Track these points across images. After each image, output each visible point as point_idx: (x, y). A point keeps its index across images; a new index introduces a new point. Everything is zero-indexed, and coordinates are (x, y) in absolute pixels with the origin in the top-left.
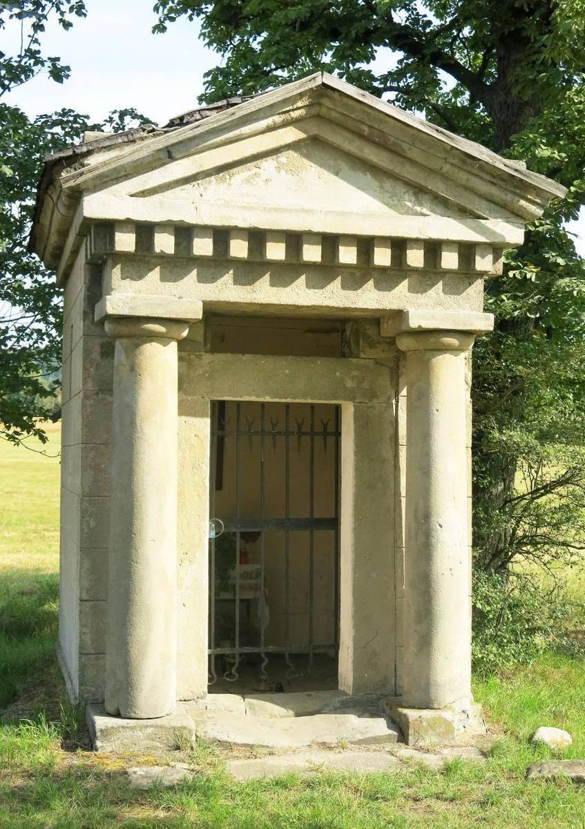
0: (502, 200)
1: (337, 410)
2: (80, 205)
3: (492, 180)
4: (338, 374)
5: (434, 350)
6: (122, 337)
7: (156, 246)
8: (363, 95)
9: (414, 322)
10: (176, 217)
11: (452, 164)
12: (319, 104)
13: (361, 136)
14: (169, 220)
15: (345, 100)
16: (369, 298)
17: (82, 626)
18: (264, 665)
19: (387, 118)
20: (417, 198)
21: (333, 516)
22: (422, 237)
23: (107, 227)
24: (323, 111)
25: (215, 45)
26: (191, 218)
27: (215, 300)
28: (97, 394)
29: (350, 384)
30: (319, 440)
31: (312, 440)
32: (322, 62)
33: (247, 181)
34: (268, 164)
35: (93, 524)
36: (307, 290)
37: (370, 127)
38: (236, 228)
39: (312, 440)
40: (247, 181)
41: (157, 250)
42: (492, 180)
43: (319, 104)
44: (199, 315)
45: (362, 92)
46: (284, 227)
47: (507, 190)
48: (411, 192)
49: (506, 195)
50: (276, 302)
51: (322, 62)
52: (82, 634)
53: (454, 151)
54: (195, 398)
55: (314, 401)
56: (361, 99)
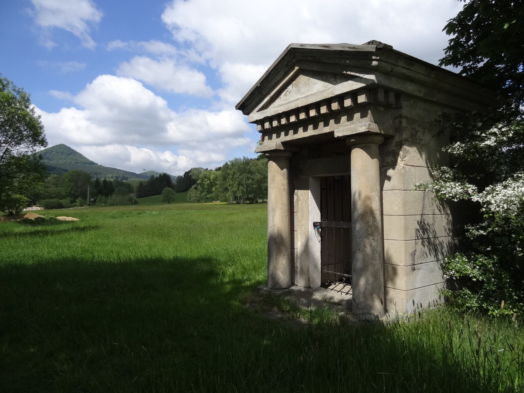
9: (336, 135)
16: (322, 129)
22: (333, 96)
34: (290, 87)
40: (285, 95)
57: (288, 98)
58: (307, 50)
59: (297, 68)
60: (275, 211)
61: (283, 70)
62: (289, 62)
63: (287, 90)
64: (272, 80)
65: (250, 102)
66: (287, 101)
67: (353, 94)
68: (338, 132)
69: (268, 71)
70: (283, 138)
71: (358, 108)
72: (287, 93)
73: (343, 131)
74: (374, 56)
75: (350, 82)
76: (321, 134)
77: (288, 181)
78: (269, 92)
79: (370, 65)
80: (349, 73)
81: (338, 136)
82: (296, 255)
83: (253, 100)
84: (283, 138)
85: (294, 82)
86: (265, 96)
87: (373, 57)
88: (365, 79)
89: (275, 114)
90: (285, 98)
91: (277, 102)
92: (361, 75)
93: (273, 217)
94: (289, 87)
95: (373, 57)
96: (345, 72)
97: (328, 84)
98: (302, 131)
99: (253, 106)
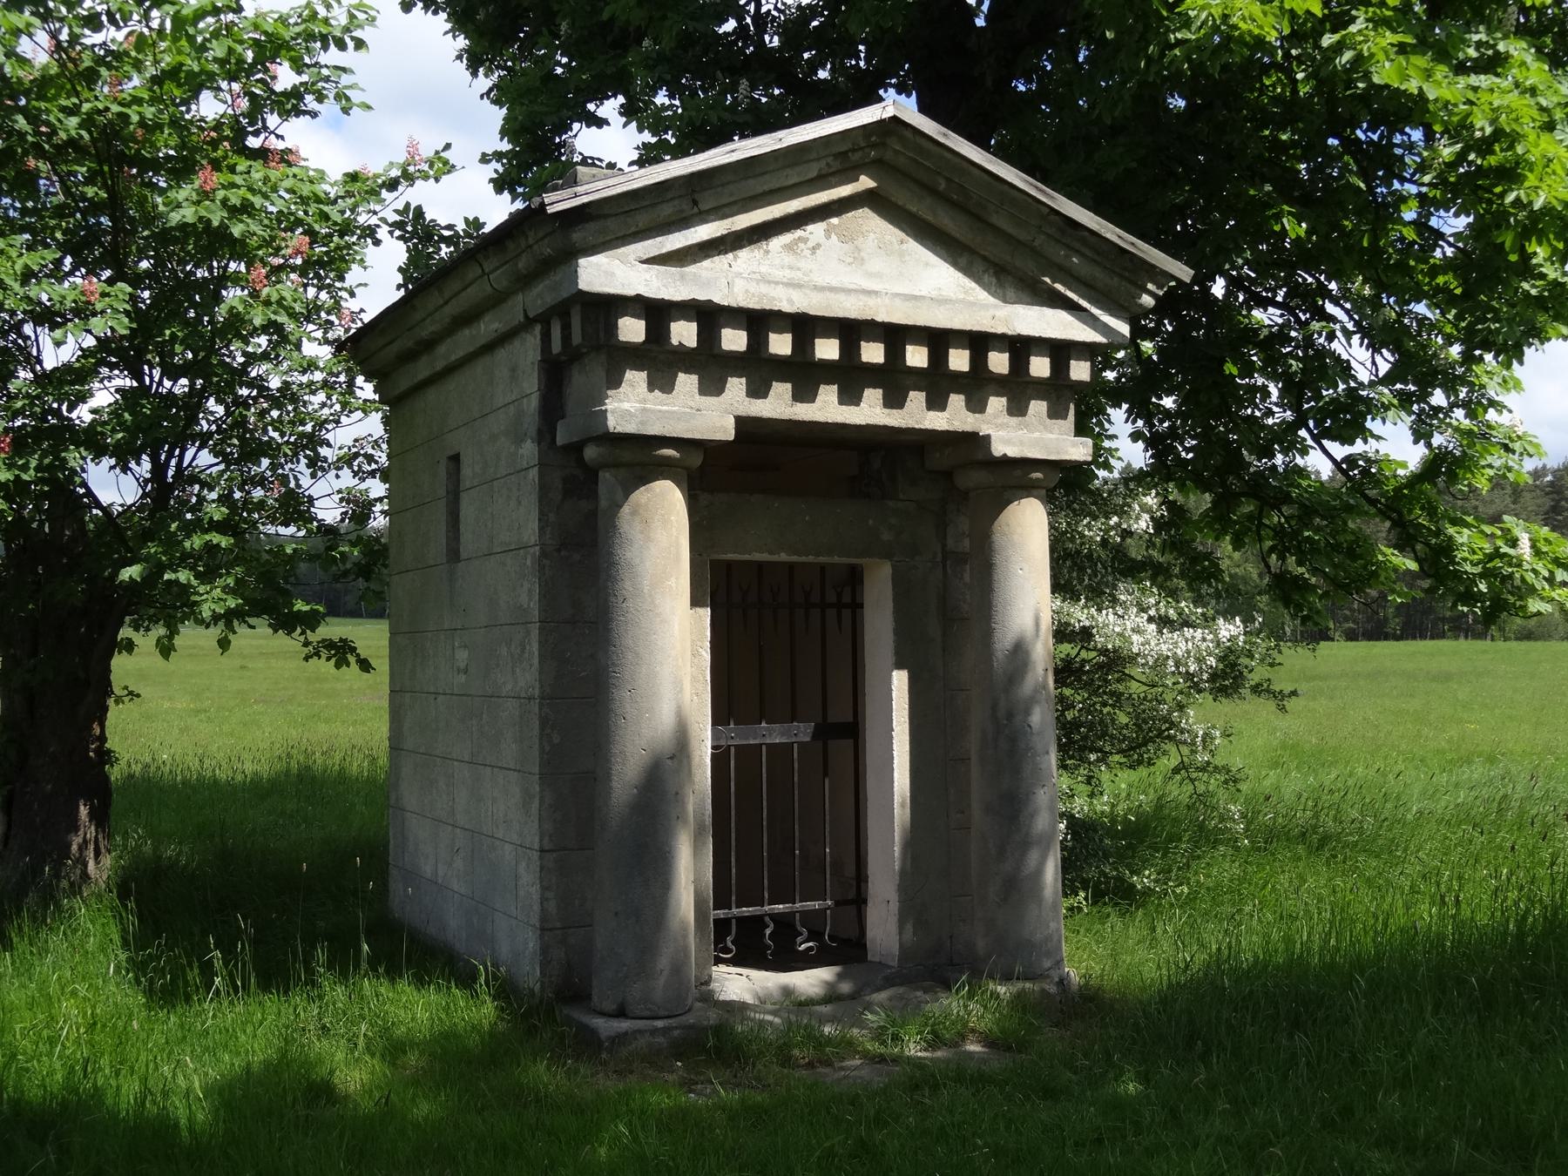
3: (1096, 257)
4: (871, 522)
5: (1011, 487)
7: (672, 336)
8: (945, 135)
11: (1049, 236)
12: (884, 144)
13: (933, 191)
14: (694, 300)
16: (954, 416)
17: (544, 889)
18: (768, 932)
19: (972, 169)
20: (998, 279)
21: (851, 719)
22: (1010, 333)
23: (612, 306)
24: (889, 156)
26: (721, 298)
28: (559, 550)
29: (886, 536)
30: (831, 614)
32: (505, 146)
33: (789, 248)
34: (816, 230)
35: (556, 739)
37: (949, 180)
38: (779, 314)
40: (789, 248)
41: (675, 342)
42: (1096, 257)
43: (884, 144)
45: (944, 130)
46: (841, 314)
48: (991, 271)
50: (822, 419)
51: (505, 146)
52: (543, 900)
53: (1052, 217)
55: (795, 558)
56: (942, 140)
57: (802, 264)
59: (865, 182)
61: (823, 164)
62: (853, 150)
63: (799, 233)
66: (797, 276)
67: (1061, 351)
68: (1008, 442)
71: (1058, 391)
72: (801, 245)
73: (1022, 443)
75: (1062, 316)
77: (611, 554)
78: (726, 210)
79: (1134, 298)
80: (1058, 286)
82: (704, 843)
84: (736, 398)
85: (835, 221)
86: (703, 217)
87: (1150, 286)
88: (1105, 325)
89: (757, 307)
90: (788, 259)
91: (746, 258)
94: (810, 228)
95: (1150, 286)
96: (1047, 280)
97: (973, 285)
98: (835, 398)
99: (633, 229)
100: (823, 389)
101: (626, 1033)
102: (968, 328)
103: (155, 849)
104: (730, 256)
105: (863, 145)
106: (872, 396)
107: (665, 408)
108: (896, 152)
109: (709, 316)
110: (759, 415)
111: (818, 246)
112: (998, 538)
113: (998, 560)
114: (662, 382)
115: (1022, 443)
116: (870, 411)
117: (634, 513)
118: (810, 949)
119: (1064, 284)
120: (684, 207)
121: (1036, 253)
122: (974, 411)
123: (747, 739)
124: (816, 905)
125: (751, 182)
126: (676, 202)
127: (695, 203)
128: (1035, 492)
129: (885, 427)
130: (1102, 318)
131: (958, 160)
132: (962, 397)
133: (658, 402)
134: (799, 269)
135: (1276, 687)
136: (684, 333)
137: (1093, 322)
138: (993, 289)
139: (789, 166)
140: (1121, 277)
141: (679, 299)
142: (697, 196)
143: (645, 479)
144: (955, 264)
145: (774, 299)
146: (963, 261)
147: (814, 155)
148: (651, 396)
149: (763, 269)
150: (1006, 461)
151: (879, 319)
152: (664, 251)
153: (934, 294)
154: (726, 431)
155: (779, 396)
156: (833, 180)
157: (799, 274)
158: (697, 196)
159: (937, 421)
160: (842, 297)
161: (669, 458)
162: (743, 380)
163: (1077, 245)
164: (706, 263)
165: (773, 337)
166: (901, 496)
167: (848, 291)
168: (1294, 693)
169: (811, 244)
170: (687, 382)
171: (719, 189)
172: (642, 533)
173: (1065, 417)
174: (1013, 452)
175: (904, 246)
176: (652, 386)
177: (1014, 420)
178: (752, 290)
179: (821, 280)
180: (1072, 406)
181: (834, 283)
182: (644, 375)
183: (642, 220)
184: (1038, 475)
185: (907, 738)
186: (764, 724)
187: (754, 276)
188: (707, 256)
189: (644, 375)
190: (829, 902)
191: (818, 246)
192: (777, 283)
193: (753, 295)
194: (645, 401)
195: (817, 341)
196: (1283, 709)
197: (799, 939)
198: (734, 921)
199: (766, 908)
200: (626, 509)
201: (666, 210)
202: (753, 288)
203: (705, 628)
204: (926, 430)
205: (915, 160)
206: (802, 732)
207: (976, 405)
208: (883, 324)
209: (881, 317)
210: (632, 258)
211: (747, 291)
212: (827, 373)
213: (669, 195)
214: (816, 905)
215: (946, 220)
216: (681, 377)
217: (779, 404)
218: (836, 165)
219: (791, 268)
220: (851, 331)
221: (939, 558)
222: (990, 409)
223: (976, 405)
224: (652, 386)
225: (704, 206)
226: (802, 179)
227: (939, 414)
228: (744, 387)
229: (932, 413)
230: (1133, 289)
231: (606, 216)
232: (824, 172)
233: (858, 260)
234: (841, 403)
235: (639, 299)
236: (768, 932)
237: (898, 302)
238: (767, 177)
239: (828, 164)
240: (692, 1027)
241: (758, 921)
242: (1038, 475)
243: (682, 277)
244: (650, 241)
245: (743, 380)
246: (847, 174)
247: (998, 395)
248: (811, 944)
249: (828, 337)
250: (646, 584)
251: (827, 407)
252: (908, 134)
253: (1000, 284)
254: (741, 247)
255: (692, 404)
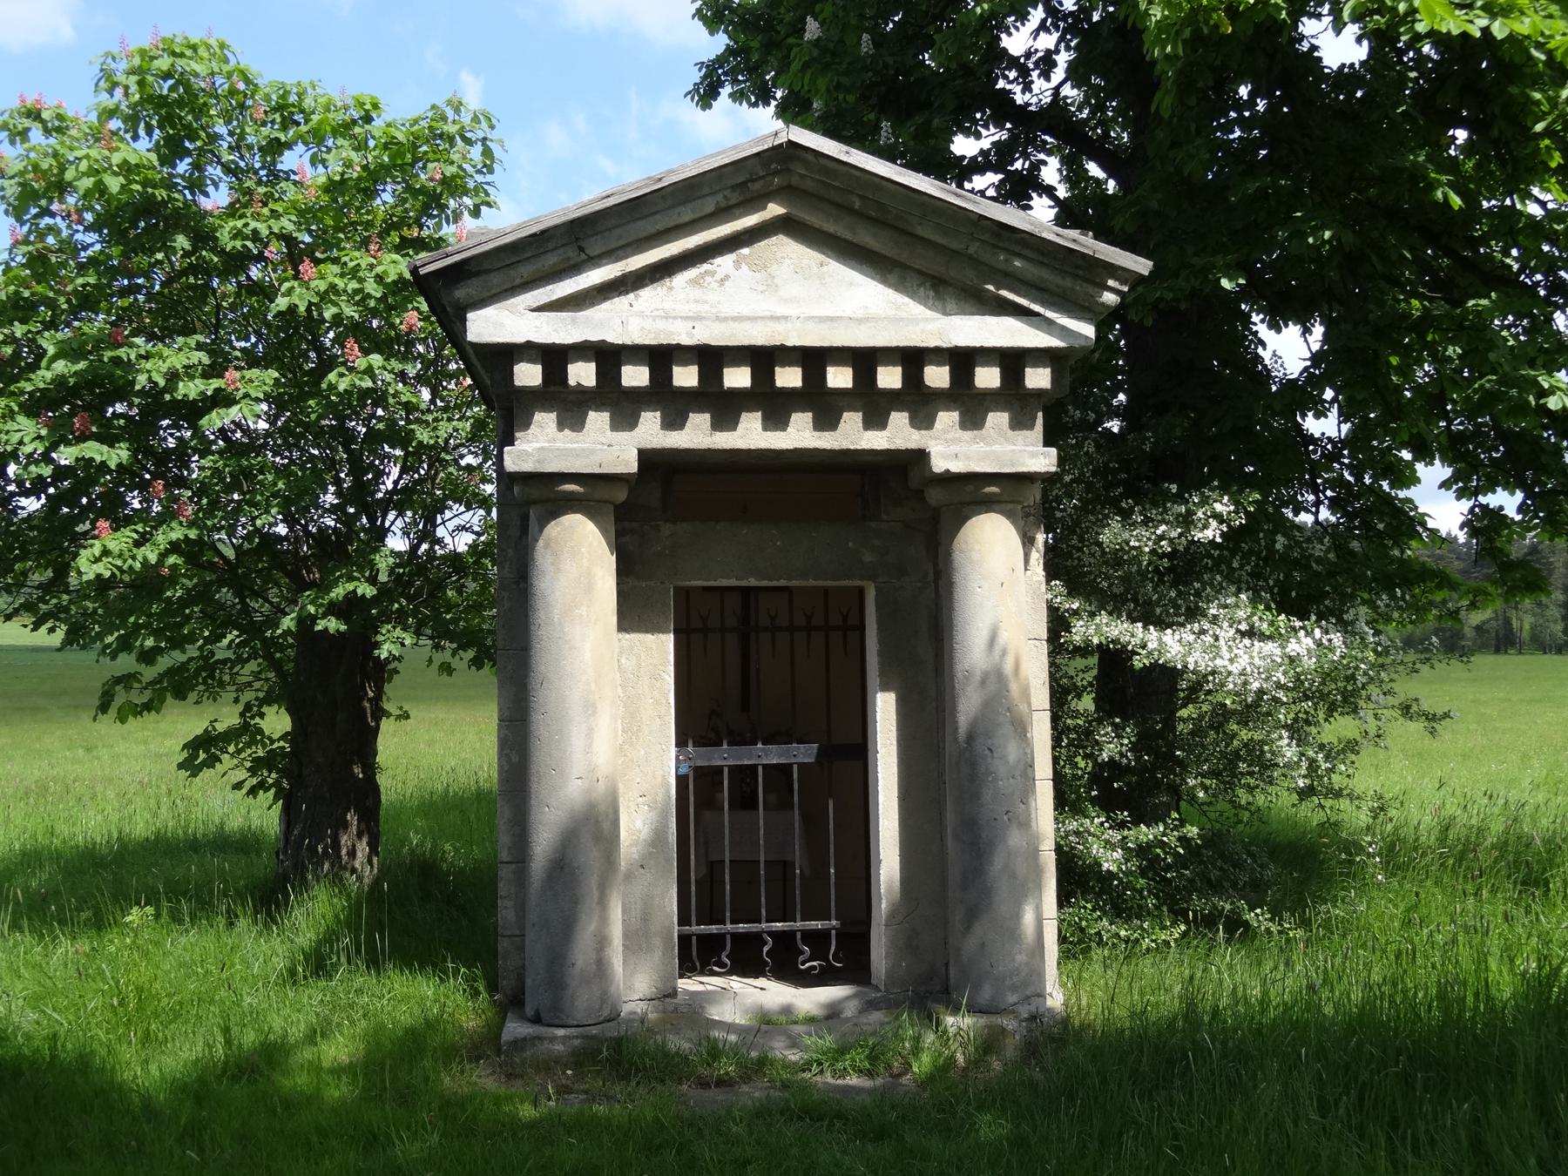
0: (1058, 287)
1: (861, 592)
2: (974, 310)
3: (1041, 259)
4: (850, 544)
6: (535, 503)
9: (939, 464)
10: (594, 337)
12: (789, 170)
13: (850, 211)
15: (823, 161)
16: (898, 433)
18: (766, 949)
19: (885, 183)
20: (936, 292)
22: (944, 345)
24: (795, 181)
25: (727, 90)
26: (614, 337)
27: (659, 447)
29: (868, 558)
31: (845, 637)
33: (695, 282)
34: (724, 263)
36: (1010, 432)
37: (861, 197)
39: (845, 637)
42: (1041, 259)
43: (789, 170)
44: (633, 467)
46: (746, 342)
47: (1066, 272)
48: (928, 284)
49: (1063, 278)
54: (652, 583)
58: (858, 173)
59: (774, 210)
60: (594, 713)
61: (720, 197)
62: (753, 181)
63: (705, 267)
64: (655, 213)
65: (508, 262)
67: (1013, 361)
68: (946, 457)
69: (660, 179)
70: (650, 431)
71: (1014, 397)
72: (708, 279)
73: (968, 458)
74: (1116, 279)
76: (849, 450)
78: (620, 253)
80: (1004, 293)
81: (947, 471)
83: (528, 258)
84: (650, 431)
85: (745, 251)
87: (1111, 283)
88: (1063, 328)
90: (694, 293)
91: (649, 297)
92: (1050, 314)
93: (590, 734)
94: (718, 261)
95: (1111, 283)
96: (991, 288)
97: (906, 300)
98: (553, 426)
99: (518, 281)
100: (745, 416)
101: (524, 1039)
102: (894, 344)
103: (434, 846)
104: (631, 296)
105: (762, 173)
106: (899, 419)
107: (575, 445)
108: (802, 176)
109: (609, 357)
110: (675, 446)
111: (727, 277)
112: (958, 557)
113: (958, 578)
114: (973, 419)
115: (968, 458)
116: (800, 434)
117: (547, 546)
118: (814, 968)
119: (1011, 290)
120: (571, 254)
121: (974, 261)
122: (919, 428)
123: (741, 759)
124: (818, 925)
125: (640, 224)
126: (561, 251)
127: (581, 249)
128: (997, 507)
129: (816, 450)
130: (1058, 321)
131: (868, 177)
132: (906, 414)
133: (568, 440)
134: (706, 302)
135: (1426, 706)
136: (582, 374)
137: (1048, 326)
138: (931, 302)
139: (679, 204)
140: (1076, 277)
141: (571, 341)
142: (582, 243)
143: (555, 514)
144: (885, 282)
145: (672, 333)
146: (892, 278)
147: (706, 190)
148: (560, 435)
149: (666, 305)
150: (949, 478)
151: (789, 343)
152: (554, 298)
153: (860, 314)
154: (627, 463)
155: (697, 427)
156: (737, 211)
157: (707, 307)
158: (582, 243)
159: (876, 440)
160: (747, 325)
161: (572, 493)
162: (658, 414)
163: (1017, 249)
164: (606, 305)
165: (677, 370)
166: (884, 517)
167: (753, 319)
168: (1446, 715)
169: (718, 277)
170: (598, 420)
171: (607, 234)
172: (552, 564)
173: (1031, 427)
174: (956, 467)
175: (825, 269)
176: (561, 425)
177: (968, 434)
178: (648, 327)
179: (727, 310)
180: (1040, 414)
181: (746, 312)
182: (553, 416)
183: (526, 271)
184: (994, 489)
185: (895, 760)
186: (760, 745)
187: (657, 313)
188: (606, 299)
189: (553, 416)
190: (834, 922)
191: (727, 277)
192: (675, 318)
193: (649, 331)
194: (554, 440)
195: (725, 370)
196: (1433, 732)
197: (801, 958)
198: (728, 937)
199: (764, 925)
200: (541, 543)
201: (551, 260)
202: (649, 324)
203: (667, 653)
204: (864, 450)
205: (822, 182)
206: (804, 753)
207: (923, 421)
208: (795, 348)
209: (791, 342)
210: (521, 308)
211: (642, 329)
212: (893, 400)
213: (551, 245)
214: (818, 925)
215: (866, 237)
216: (592, 415)
217: (697, 434)
218: (735, 198)
219: (696, 301)
220: (763, 359)
221: (931, 577)
222: (938, 425)
223: (923, 421)
224: (561, 425)
225: (593, 252)
226: (697, 215)
227: (878, 433)
228: (659, 419)
229: (870, 433)
230: (1091, 290)
231: (487, 272)
232: (723, 204)
233: (771, 286)
234: (765, 429)
235: (529, 345)
236: (766, 949)
237: (811, 325)
238: (658, 216)
239: (725, 197)
240: (593, 1037)
241: (757, 938)
242: (994, 489)
243: (574, 320)
244: (540, 290)
245: (658, 414)
246: (754, 202)
247: (948, 410)
248: (814, 963)
249: (738, 365)
250: (556, 613)
251: (750, 434)
252: (810, 157)
253: (939, 296)
254: (643, 286)
255: (604, 440)
